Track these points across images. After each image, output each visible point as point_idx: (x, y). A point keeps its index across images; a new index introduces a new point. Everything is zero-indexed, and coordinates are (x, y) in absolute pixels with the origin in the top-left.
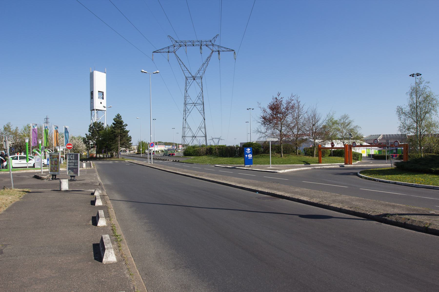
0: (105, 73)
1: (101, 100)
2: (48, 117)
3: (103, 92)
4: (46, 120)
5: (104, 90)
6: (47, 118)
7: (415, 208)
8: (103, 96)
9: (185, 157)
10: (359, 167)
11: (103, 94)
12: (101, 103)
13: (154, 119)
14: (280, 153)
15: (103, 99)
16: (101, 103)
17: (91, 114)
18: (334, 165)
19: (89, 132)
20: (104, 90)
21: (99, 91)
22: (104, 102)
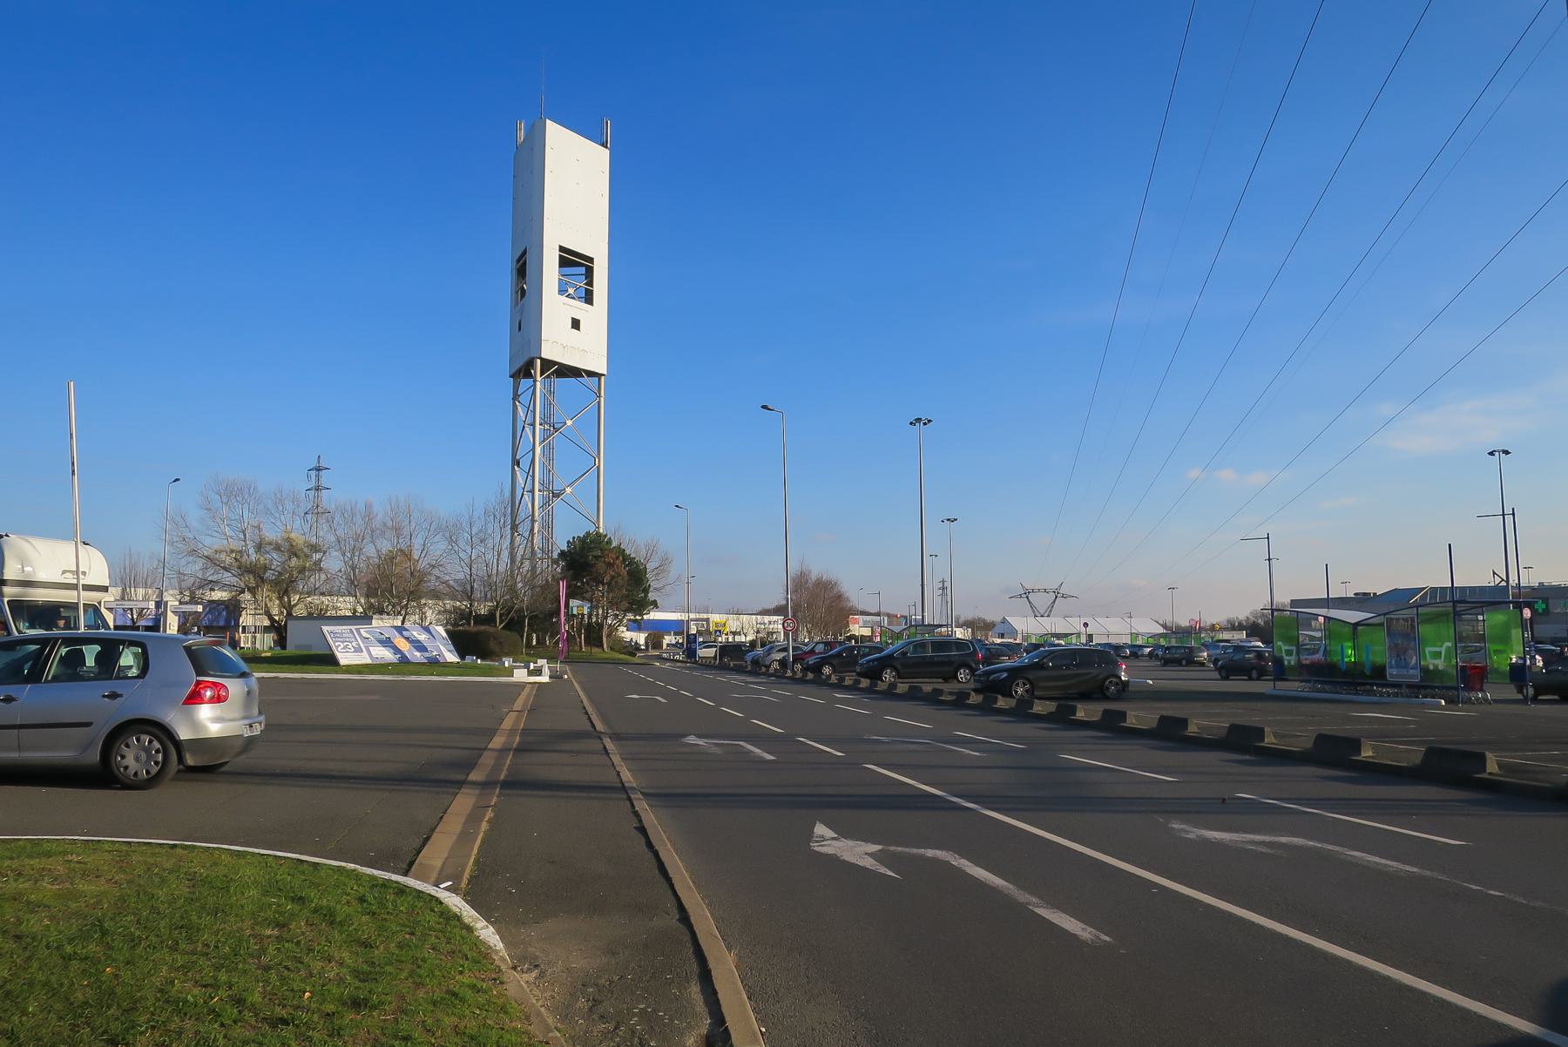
0: (604, 145)
1: (578, 309)
2: (323, 464)
3: (591, 260)
4: (313, 477)
5: (595, 244)
6: (318, 469)
7: (1517, 899)
8: (590, 283)
9: (1164, 668)
10: (306, 667)
11: (589, 273)
12: (576, 324)
13: (919, 420)
14: (100, 673)
15: (589, 299)
16: (576, 324)
17: (516, 397)
18: (359, 673)
19: (593, 259)
20: (595, 244)
21: (562, 249)
22: (596, 316)
